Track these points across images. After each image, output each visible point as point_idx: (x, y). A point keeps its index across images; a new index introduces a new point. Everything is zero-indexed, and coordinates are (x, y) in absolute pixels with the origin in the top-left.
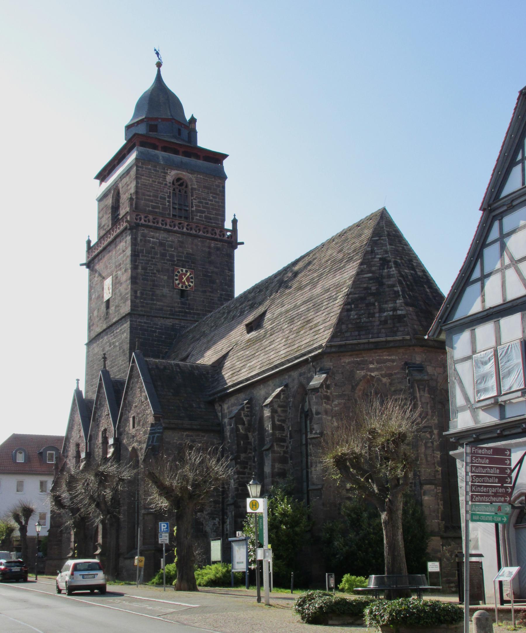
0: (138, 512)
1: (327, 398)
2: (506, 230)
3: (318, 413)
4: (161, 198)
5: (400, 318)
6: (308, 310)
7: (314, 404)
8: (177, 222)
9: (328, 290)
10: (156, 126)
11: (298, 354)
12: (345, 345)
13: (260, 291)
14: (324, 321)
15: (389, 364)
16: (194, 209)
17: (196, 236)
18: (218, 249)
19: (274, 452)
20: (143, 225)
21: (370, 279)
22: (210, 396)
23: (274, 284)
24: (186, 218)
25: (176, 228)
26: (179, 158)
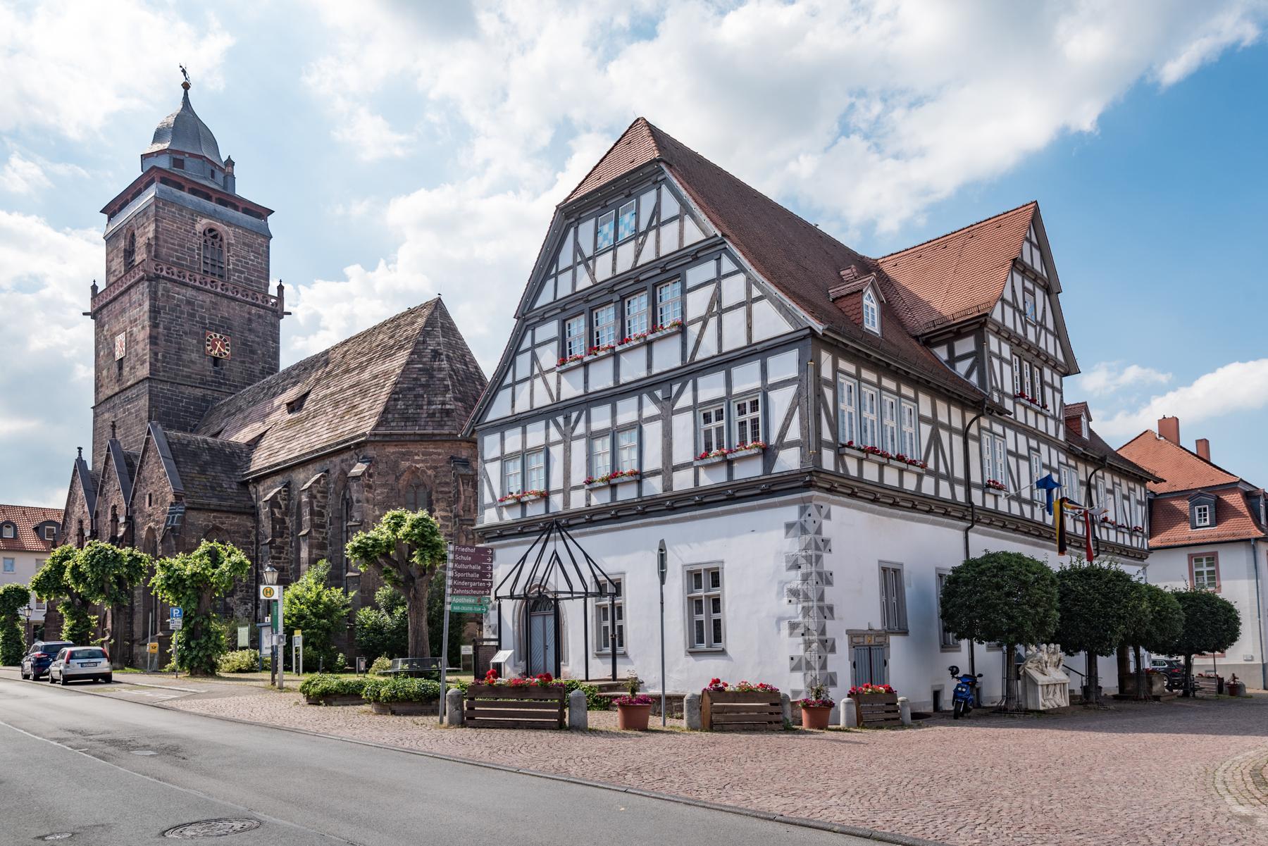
1: (370, 487)
2: (537, 341)
3: (358, 501)
5: (448, 413)
7: (355, 492)
8: (209, 280)
12: (391, 435)
15: (434, 457)
18: (260, 316)
20: (164, 278)
21: (420, 369)
24: (221, 276)
25: (208, 287)
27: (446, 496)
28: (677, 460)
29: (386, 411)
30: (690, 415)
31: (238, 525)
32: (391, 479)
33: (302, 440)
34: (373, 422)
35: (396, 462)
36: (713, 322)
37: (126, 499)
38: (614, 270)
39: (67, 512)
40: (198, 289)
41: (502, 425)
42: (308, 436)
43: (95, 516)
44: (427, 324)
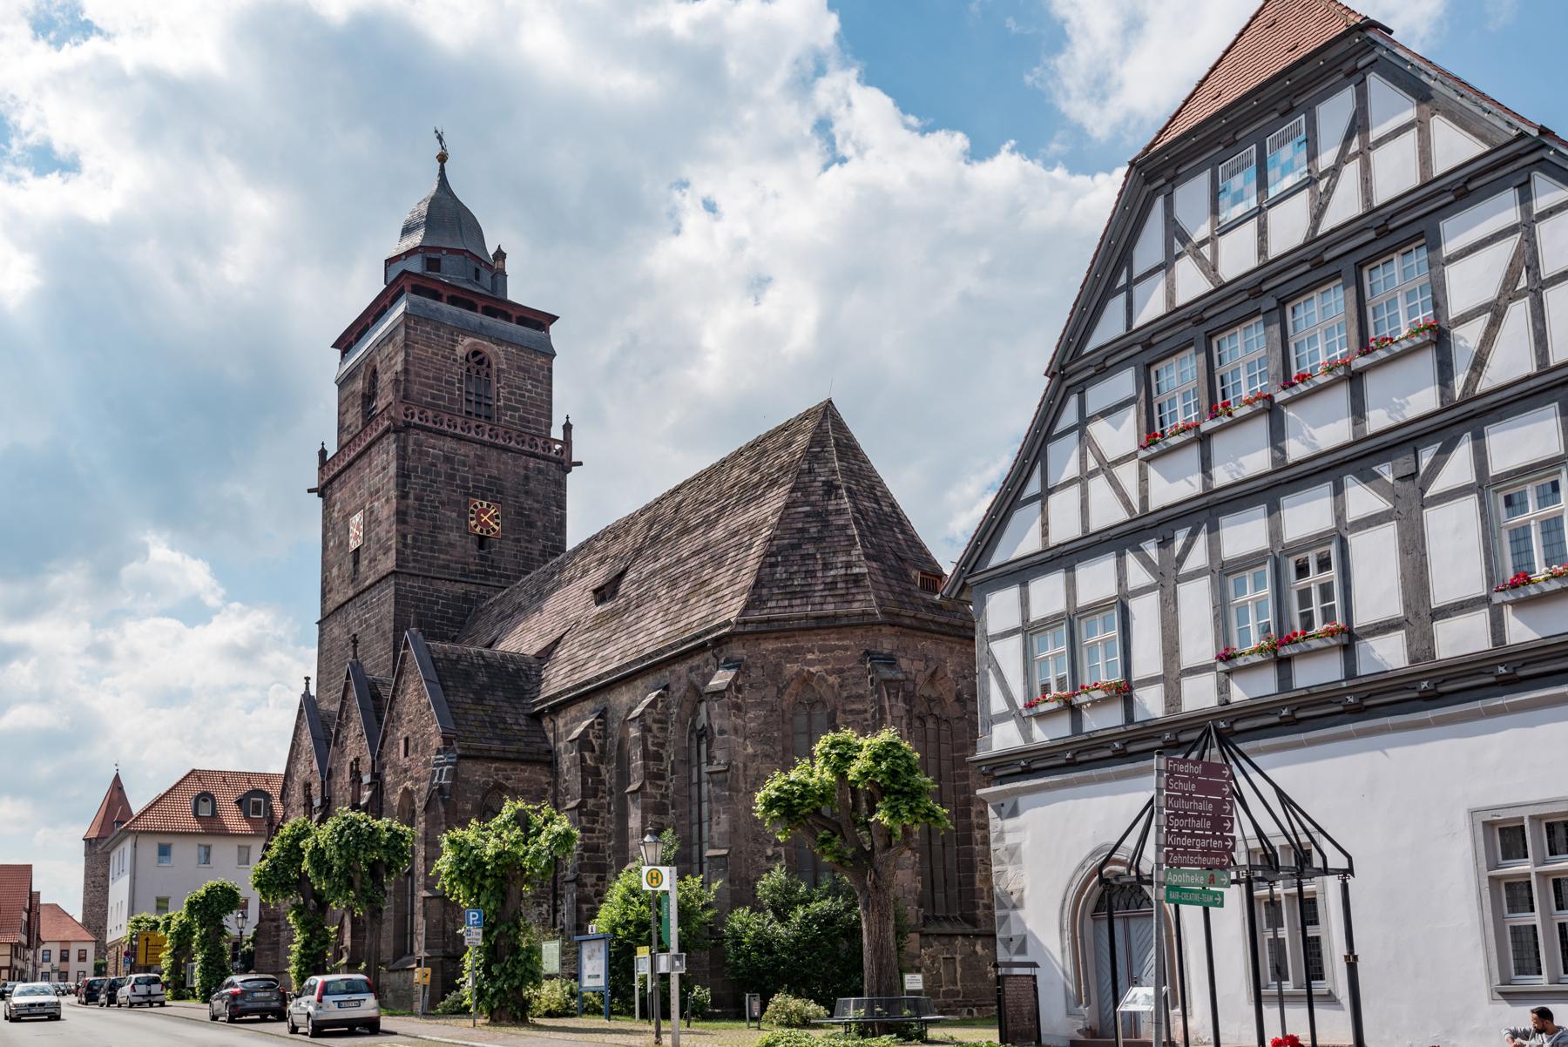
0: (413, 895)
1: (738, 707)
3: (722, 732)
4: (447, 382)
5: (857, 580)
6: (702, 566)
8: (473, 424)
9: (735, 533)
10: (438, 260)
11: (687, 635)
13: (616, 537)
14: (731, 583)
16: (501, 403)
17: (506, 449)
18: (540, 471)
19: (645, 795)
20: (416, 426)
21: (807, 514)
22: (534, 705)
23: (638, 527)
24: (488, 418)
25: (472, 434)
26: (476, 317)
27: (859, 718)
28: (1441, 595)
29: (758, 584)
30: (1470, 503)
31: (528, 780)
32: (770, 694)
33: (624, 642)
34: (739, 603)
35: (778, 665)
36: (1519, 312)
37: (372, 747)
38: (1262, 251)
39: (288, 775)
40: (459, 438)
41: (1022, 569)
42: (631, 635)
43: (328, 775)
44: (814, 441)
